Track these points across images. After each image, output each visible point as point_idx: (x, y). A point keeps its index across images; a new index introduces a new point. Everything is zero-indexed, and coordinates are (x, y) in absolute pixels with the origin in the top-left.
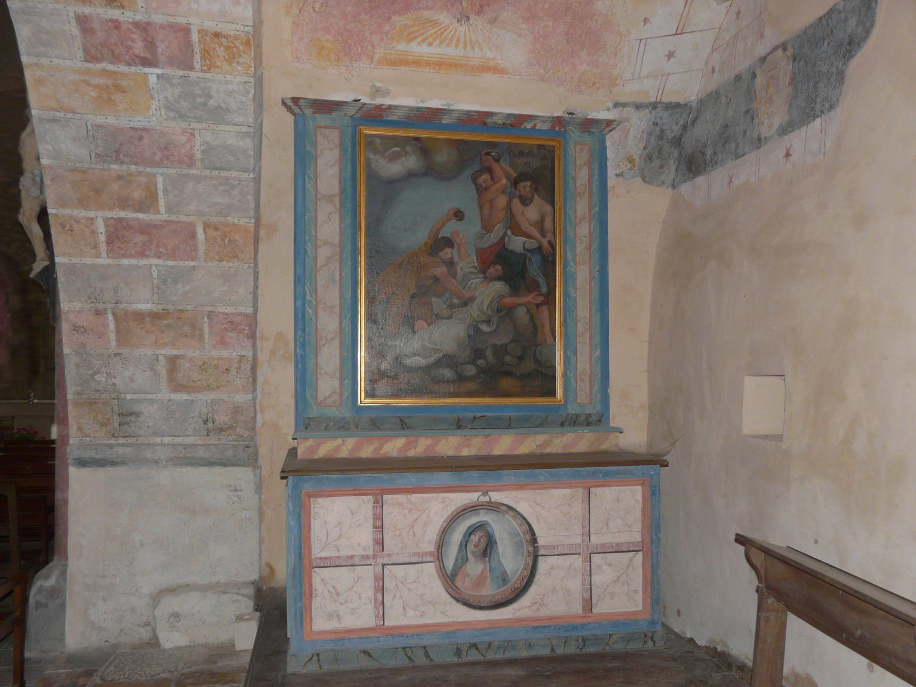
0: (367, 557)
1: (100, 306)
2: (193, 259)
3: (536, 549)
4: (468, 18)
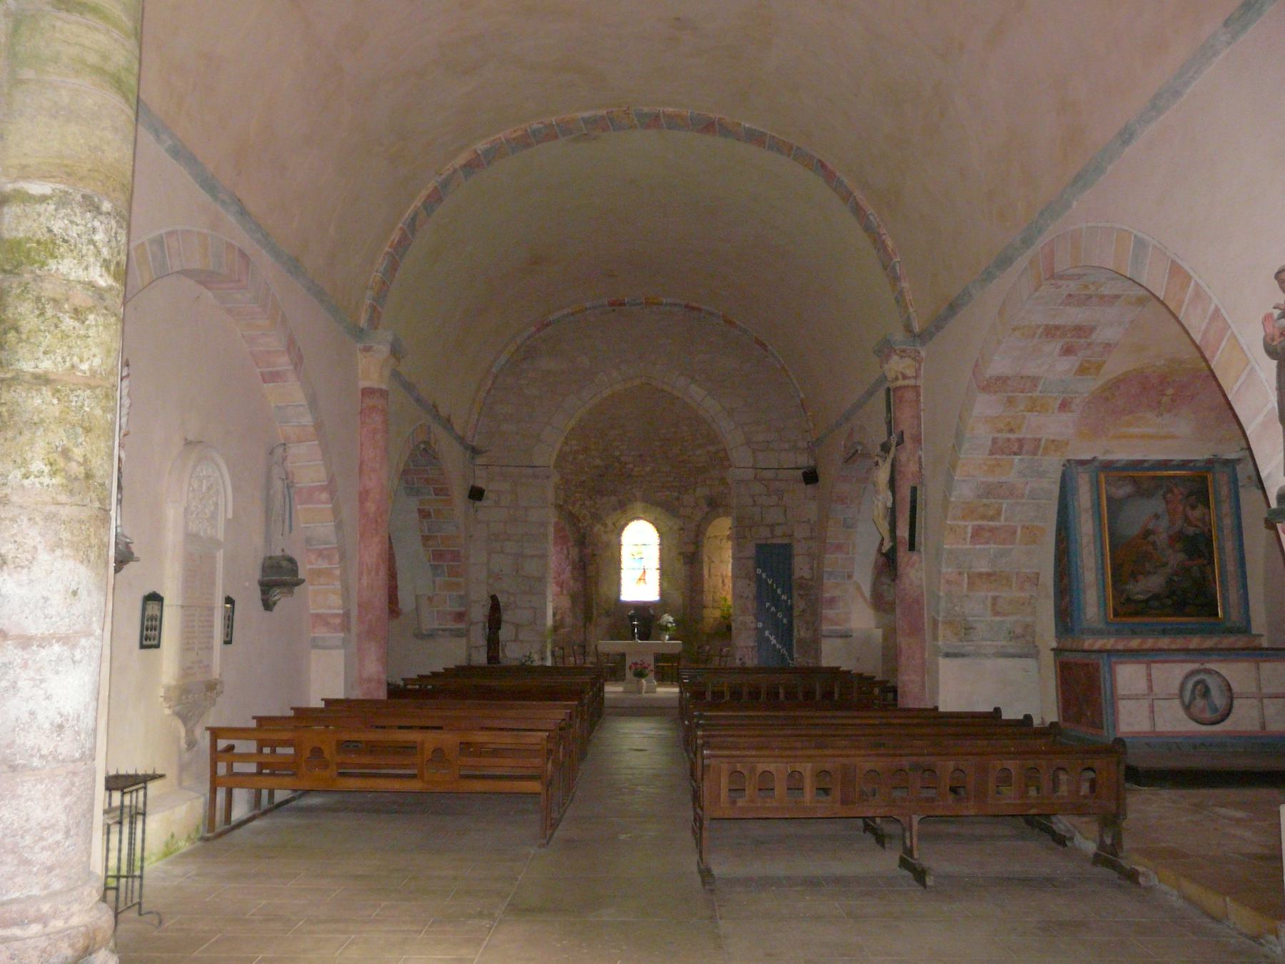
0: (1145, 695)
1: (961, 570)
2: (1013, 544)
3: (1231, 694)
4: (1162, 415)
